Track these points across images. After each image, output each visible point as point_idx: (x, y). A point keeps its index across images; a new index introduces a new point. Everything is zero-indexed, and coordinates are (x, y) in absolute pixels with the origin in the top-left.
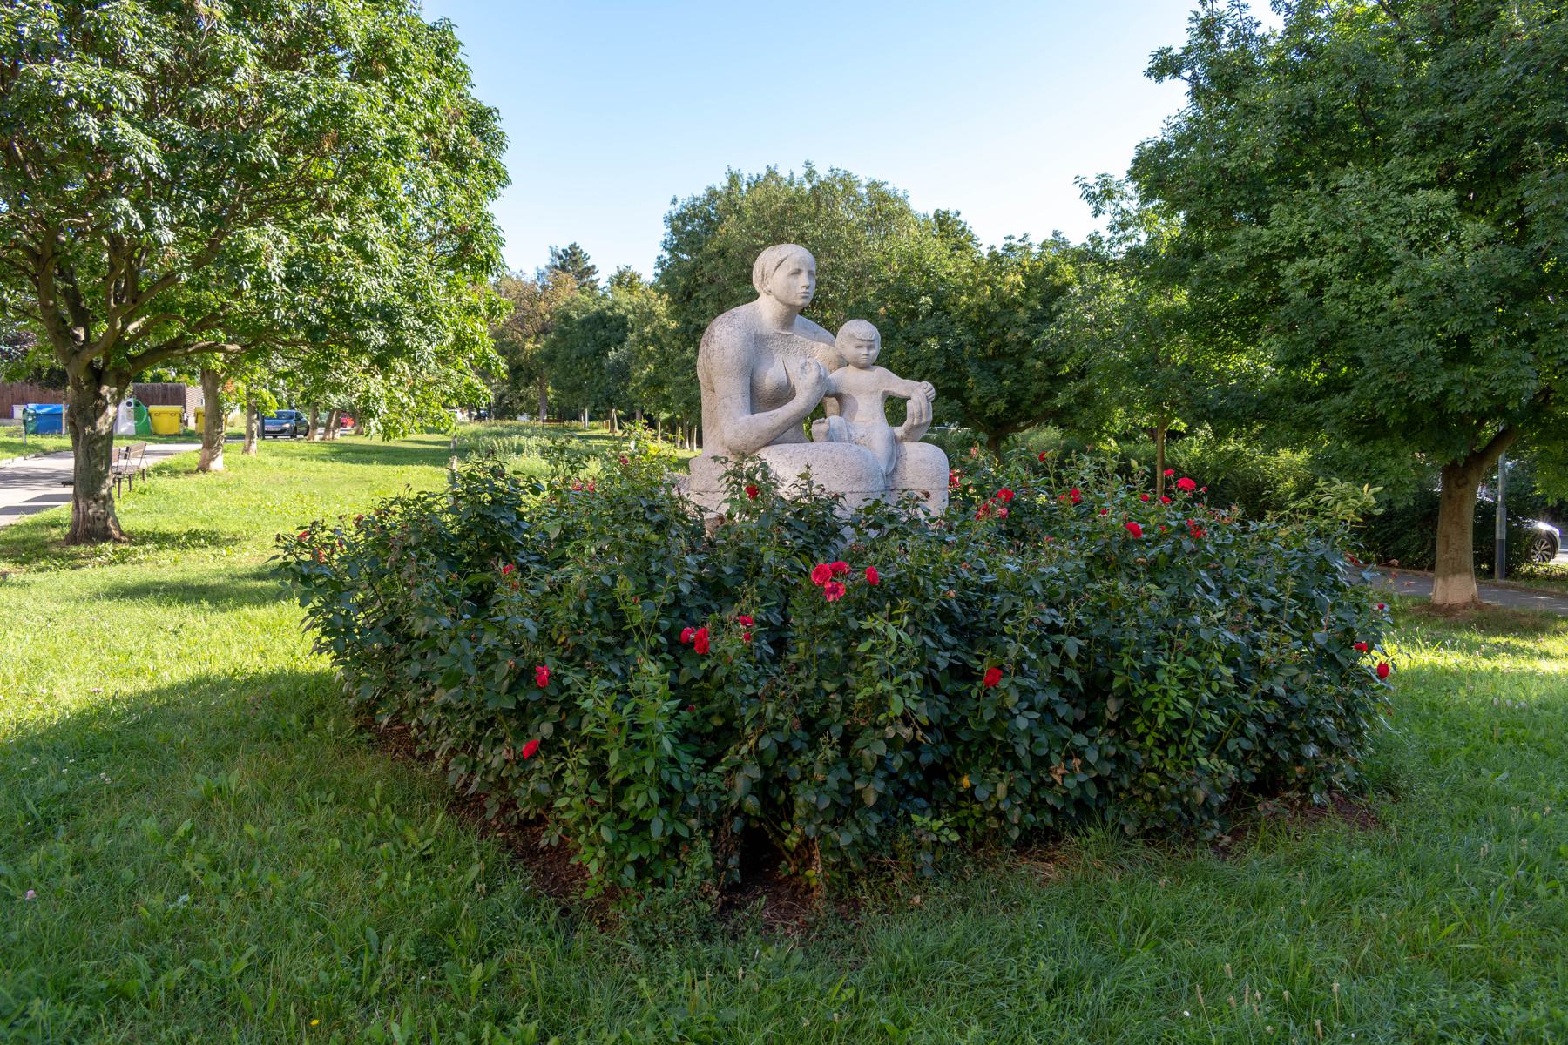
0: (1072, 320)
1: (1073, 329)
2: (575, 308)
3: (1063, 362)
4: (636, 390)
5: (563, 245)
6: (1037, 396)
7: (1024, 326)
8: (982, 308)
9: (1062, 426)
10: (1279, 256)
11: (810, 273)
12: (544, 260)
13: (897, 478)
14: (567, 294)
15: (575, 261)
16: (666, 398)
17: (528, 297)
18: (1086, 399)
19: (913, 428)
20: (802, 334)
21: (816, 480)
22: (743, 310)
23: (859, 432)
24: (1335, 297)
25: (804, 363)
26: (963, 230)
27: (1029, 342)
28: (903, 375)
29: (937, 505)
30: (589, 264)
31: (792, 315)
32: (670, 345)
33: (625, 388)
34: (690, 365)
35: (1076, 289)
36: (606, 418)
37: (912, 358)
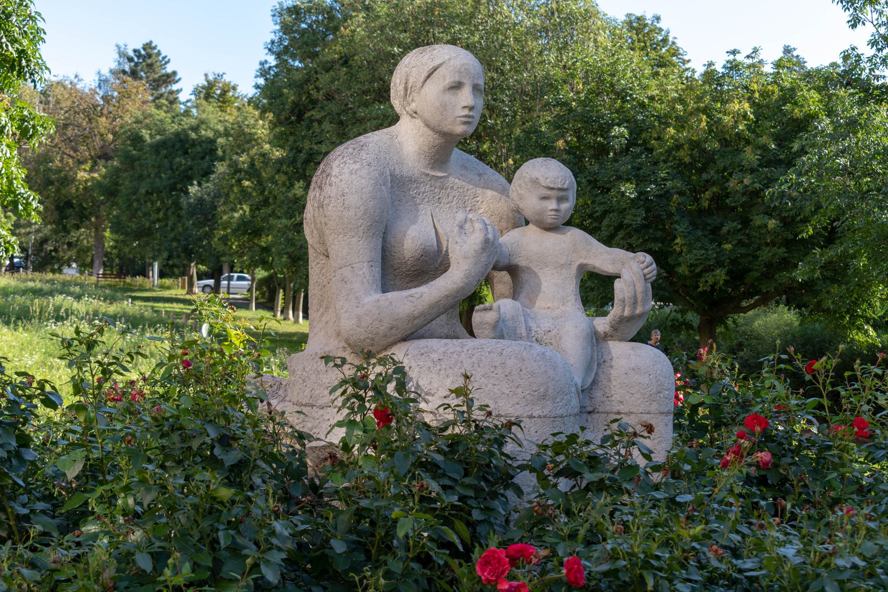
0: (819, 164)
1: (820, 177)
2: (147, 127)
3: (806, 220)
4: (224, 240)
5: (135, 43)
6: (769, 265)
7: (752, 171)
8: (695, 145)
9: (799, 307)
11: (475, 88)
12: (108, 62)
13: (598, 394)
14: (138, 106)
15: (150, 66)
16: (266, 250)
17: (77, 114)
18: (836, 272)
21: (480, 398)
22: (375, 139)
23: (542, 324)
25: (461, 220)
26: (665, 41)
27: (756, 194)
28: (608, 241)
29: (662, 443)
30: (169, 69)
31: (445, 147)
32: (272, 180)
33: (209, 236)
34: (298, 205)
36: (183, 274)
37: (599, 209)
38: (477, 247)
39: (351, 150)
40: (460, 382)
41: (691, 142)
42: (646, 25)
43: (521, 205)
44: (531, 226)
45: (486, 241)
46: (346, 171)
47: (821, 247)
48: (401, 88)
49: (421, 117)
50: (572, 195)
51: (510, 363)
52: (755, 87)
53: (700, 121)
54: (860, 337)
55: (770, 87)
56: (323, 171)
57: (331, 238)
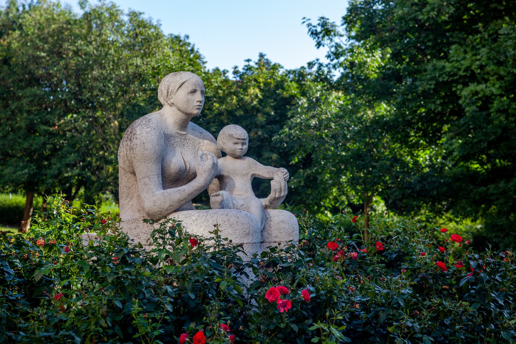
0: (301, 124)
1: (301, 130)
3: (294, 154)
7: (262, 127)
10: (457, 82)
13: (265, 234)
19: (275, 199)
21: (223, 235)
22: (154, 116)
24: (498, 111)
26: (192, 50)
38: (210, 167)
40: (213, 229)
41: (227, 110)
42: (180, 41)
43: (224, 147)
44: (228, 157)
45: (214, 164)
46: (144, 132)
47: (302, 168)
48: (165, 92)
49: (176, 106)
51: (232, 219)
52: (261, 80)
53: (232, 99)
54: (324, 218)
55: (269, 80)
56: (131, 132)
57: (137, 164)
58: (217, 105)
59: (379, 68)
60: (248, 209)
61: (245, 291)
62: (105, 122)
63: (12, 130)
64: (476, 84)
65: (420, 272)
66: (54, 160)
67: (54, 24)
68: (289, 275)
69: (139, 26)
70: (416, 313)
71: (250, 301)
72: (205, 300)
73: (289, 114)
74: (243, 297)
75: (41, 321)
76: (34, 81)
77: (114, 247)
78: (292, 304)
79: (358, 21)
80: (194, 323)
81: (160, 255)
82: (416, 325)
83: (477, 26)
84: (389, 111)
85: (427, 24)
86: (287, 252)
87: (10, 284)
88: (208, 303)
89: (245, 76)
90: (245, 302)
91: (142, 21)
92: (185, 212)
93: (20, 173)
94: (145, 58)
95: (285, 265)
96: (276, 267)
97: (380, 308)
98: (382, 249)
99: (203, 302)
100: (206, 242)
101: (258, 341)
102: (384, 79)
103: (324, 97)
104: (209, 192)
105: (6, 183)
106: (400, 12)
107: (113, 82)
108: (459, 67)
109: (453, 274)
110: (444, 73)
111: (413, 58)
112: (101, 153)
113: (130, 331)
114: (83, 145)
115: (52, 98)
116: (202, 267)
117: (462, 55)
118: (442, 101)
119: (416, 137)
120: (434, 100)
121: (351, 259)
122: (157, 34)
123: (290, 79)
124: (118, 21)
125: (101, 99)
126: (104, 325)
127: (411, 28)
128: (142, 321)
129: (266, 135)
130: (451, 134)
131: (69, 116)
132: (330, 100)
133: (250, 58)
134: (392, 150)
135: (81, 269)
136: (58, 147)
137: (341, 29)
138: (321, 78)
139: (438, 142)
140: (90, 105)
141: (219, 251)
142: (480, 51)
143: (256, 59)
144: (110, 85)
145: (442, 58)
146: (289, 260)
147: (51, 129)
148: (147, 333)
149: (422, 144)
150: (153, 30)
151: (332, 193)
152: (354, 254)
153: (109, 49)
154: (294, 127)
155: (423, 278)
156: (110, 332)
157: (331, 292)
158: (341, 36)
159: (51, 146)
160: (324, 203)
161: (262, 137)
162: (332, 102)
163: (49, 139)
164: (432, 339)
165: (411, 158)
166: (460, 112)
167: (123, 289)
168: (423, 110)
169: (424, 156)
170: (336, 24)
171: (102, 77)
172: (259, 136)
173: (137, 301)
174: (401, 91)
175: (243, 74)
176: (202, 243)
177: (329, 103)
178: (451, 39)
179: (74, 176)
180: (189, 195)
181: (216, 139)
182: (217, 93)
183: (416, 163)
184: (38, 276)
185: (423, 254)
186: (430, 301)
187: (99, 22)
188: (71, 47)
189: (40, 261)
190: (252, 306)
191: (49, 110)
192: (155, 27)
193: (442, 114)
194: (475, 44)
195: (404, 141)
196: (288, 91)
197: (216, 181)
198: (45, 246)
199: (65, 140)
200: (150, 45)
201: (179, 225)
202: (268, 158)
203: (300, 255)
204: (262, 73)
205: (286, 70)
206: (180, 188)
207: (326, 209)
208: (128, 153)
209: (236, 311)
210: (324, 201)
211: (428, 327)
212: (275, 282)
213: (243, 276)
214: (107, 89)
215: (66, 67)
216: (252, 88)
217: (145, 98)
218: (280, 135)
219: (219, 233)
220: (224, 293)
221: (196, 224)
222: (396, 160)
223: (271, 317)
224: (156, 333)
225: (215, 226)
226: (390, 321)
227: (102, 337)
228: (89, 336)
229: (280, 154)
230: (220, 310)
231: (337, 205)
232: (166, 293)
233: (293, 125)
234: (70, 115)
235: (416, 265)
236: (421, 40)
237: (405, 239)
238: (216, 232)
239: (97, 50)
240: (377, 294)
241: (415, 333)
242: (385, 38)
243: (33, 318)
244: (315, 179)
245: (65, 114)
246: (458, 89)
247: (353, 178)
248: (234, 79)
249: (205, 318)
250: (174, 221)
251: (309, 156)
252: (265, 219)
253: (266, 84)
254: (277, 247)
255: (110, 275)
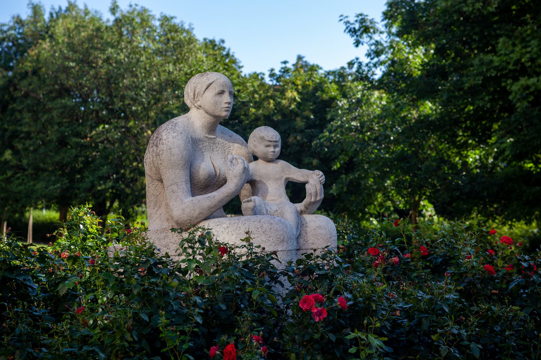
0: (341, 126)
1: (342, 133)
7: (302, 131)
10: (506, 76)
11: (230, 93)
13: (301, 241)
19: (311, 204)
20: (222, 138)
21: (255, 242)
22: (181, 120)
26: (228, 55)
35: (343, 103)
38: (241, 171)
39: (170, 126)
40: (246, 236)
41: (264, 115)
42: (216, 45)
43: (256, 150)
44: (260, 161)
45: (245, 168)
47: (345, 174)
48: (192, 94)
49: (203, 109)
50: (280, 144)
51: (265, 226)
52: (299, 82)
53: (269, 103)
55: (307, 83)
57: (164, 171)
58: (253, 110)
59: (422, 65)
60: (282, 215)
61: (280, 302)
62: (138, 132)
63: (44, 143)
64: (526, 78)
65: (467, 277)
66: (86, 174)
67: (84, 32)
68: (326, 283)
69: (170, 31)
70: (462, 320)
71: (286, 312)
72: (238, 311)
73: (329, 117)
74: (278, 307)
75: (65, 337)
76: (65, 91)
77: (140, 257)
78: (328, 313)
79: (399, 16)
80: (227, 336)
81: (189, 265)
82: (463, 332)
83: (525, 18)
84: (436, 110)
85: (472, 16)
86: (324, 259)
87: (34, 299)
88: (240, 314)
89: (282, 79)
90: (281, 312)
91: (174, 26)
92: (216, 220)
93: (52, 187)
94: (177, 64)
95: (321, 272)
96: (313, 275)
97: (423, 315)
98: (427, 254)
99: (236, 313)
100: (237, 251)
101: (293, 352)
102: (428, 76)
103: (366, 97)
104: (241, 198)
105: (38, 199)
106: (444, 4)
107: (145, 90)
108: (508, 60)
109: (503, 277)
110: (492, 68)
111: (458, 53)
112: (135, 164)
113: (158, 345)
114: (116, 157)
115: (83, 109)
116: (233, 277)
117: (511, 48)
118: (491, 97)
119: (465, 136)
120: (482, 96)
121: (393, 265)
122: (190, 39)
123: (330, 81)
124: (150, 27)
125: (134, 108)
126: (130, 339)
127: (455, 20)
128: (170, 334)
129: (305, 140)
130: (501, 132)
131: (101, 127)
132: (372, 100)
133: (287, 59)
134: (438, 152)
135: (107, 282)
136: (90, 160)
137: (381, 25)
138: (361, 77)
139: (488, 141)
140: (122, 115)
141: (252, 259)
142: (531, 44)
143: (293, 60)
144: (142, 94)
145: (489, 52)
146: (326, 268)
147: (82, 141)
148: (175, 347)
149: (471, 144)
150: (185, 34)
151: (376, 199)
152: (395, 259)
153: (141, 55)
154: (335, 131)
155: (469, 283)
156: (137, 346)
157: (369, 298)
158: (381, 33)
159: (83, 159)
160: (369, 209)
161: (301, 142)
162: (374, 103)
163: (81, 151)
164: (480, 347)
165: (460, 159)
166: (510, 108)
167: (150, 302)
168: (471, 108)
169: (473, 156)
170: (375, 20)
171: (134, 85)
172: (298, 141)
173: (164, 313)
174: (446, 88)
175: (280, 77)
176: (233, 251)
177: (370, 104)
178: (498, 32)
179: (108, 189)
180: (219, 202)
181: (247, 142)
182: (253, 97)
183: (465, 164)
184: (63, 290)
185: (469, 257)
186: (478, 306)
187: (130, 29)
188: (102, 56)
189: (66, 275)
190: (288, 316)
191: (81, 121)
192: (188, 32)
193: (491, 111)
194: (524, 35)
195: (452, 141)
196: (327, 93)
197: (248, 186)
198: (69, 258)
199: (97, 152)
200: (181, 51)
201: (208, 233)
202: (308, 164)
203: (337, 261)
204: (300, 75)
205: (326, 72)
206: (209, 195)
207: (371, 216)
208: (155, 159)
209: (270, 321)
210: (368, 207)
211: (477, 334)
212: (312, 291)
213: (278, 285)
214: (139, 97)
215: (96, 77)
216: (289, 91)
217: (178, 105)
218: (320, 139)
219: (251, 241)
220: (257, 303)
221: (226, 232)
222: (442, 161)
223: (306, 327)
224: (185, 347)
225: (247, 233)
226: (435, 329)
227: (128, 353)
228: (114, 351)
229: (320, 159)
230: (252, 321)
231: (382, 211)
232: (195, 305)
233: (334, 128)
234: (102, 126)
235: (463, 269)
236: (466, 33)
237: (451, 242)
238: (247, 240)
239: (128, 57)
240: (420, 300)
241: (462, 340)
242: (428, 33)
243: (57, 333)
244: (359, 185)
245: (97, 125)
246: (507, 84)
247: (399, 182)
248: (271, 83)
249: (236, 330)
250: (204, 229)
251: (351, 159)
252: (301, 225)
253: (304, 86)
254: (312, 254)
255: (135, 287)
